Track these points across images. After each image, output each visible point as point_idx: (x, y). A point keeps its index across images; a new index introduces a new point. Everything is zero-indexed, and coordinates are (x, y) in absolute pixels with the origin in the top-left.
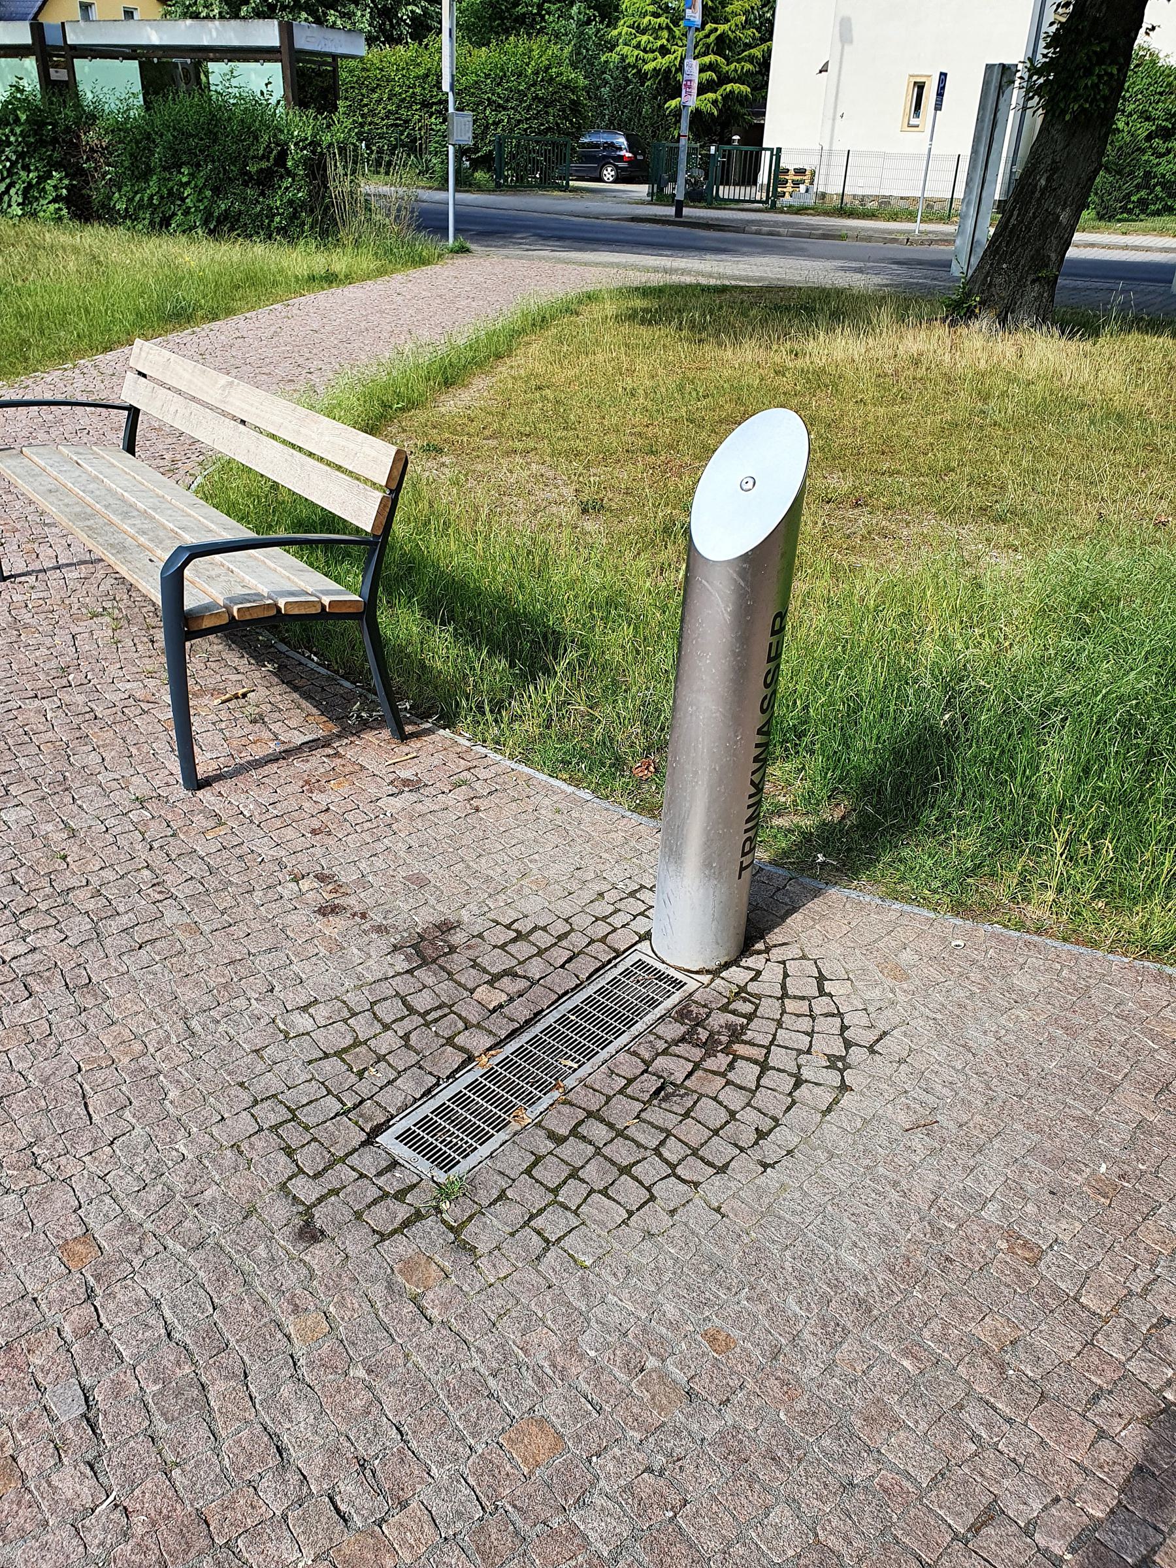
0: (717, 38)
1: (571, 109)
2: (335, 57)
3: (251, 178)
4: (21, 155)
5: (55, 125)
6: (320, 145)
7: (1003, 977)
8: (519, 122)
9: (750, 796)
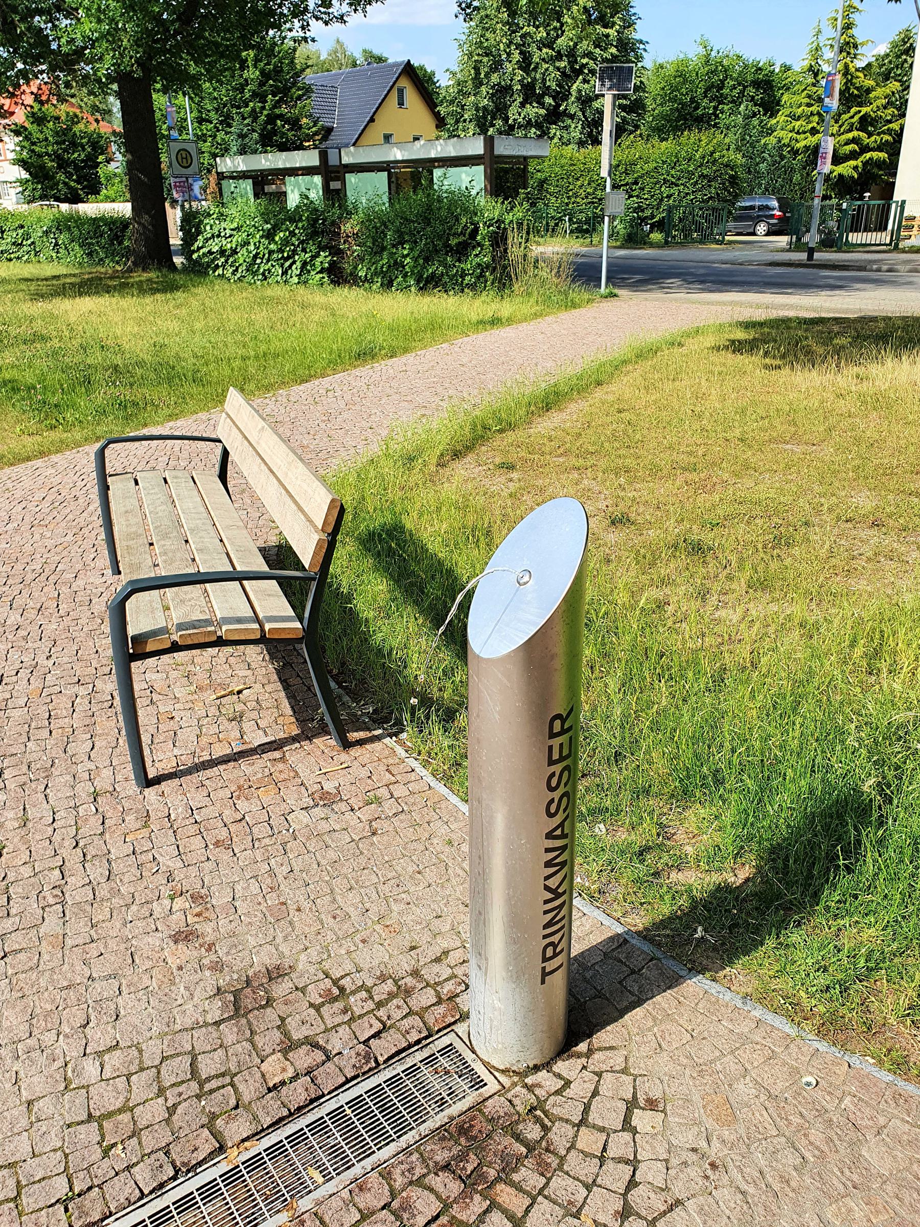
0: (861, 118)
1: (730, 182)
2: (525, 158)
3: (452, 249)
4: (302, 242)
5: (324, 220)
6: (503, 222)
7: (851, 1144)
8: (687, 194)
9: (546, 902)
